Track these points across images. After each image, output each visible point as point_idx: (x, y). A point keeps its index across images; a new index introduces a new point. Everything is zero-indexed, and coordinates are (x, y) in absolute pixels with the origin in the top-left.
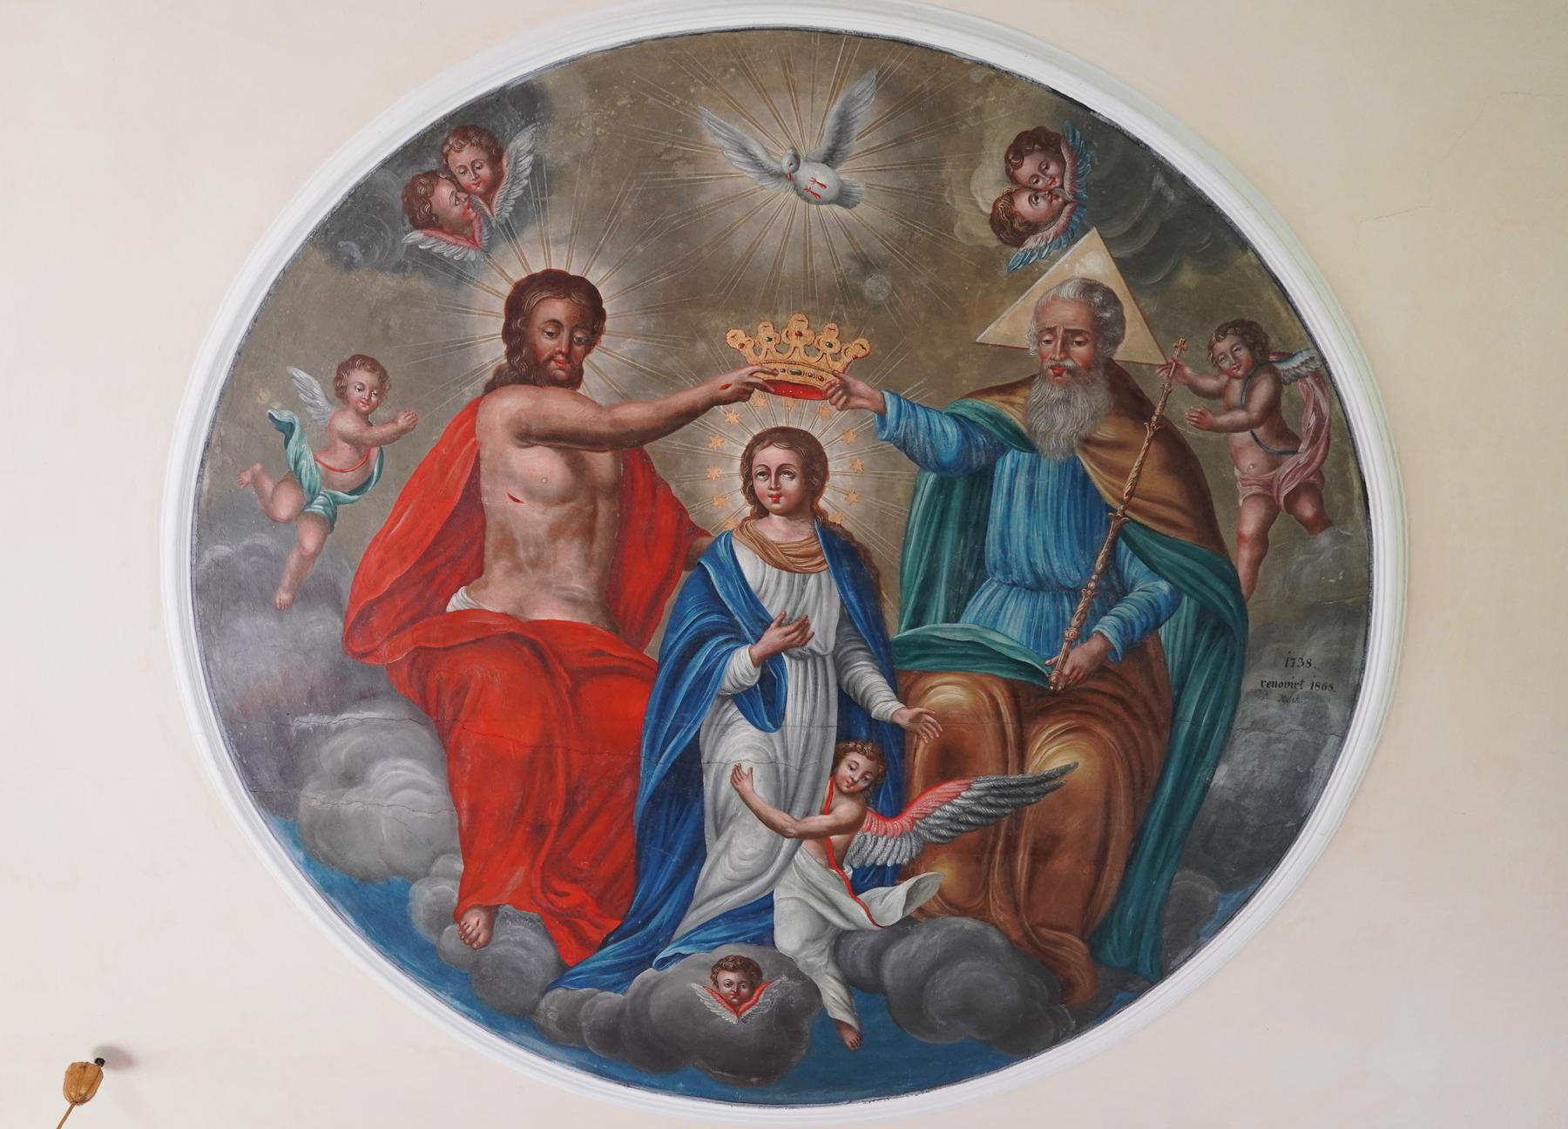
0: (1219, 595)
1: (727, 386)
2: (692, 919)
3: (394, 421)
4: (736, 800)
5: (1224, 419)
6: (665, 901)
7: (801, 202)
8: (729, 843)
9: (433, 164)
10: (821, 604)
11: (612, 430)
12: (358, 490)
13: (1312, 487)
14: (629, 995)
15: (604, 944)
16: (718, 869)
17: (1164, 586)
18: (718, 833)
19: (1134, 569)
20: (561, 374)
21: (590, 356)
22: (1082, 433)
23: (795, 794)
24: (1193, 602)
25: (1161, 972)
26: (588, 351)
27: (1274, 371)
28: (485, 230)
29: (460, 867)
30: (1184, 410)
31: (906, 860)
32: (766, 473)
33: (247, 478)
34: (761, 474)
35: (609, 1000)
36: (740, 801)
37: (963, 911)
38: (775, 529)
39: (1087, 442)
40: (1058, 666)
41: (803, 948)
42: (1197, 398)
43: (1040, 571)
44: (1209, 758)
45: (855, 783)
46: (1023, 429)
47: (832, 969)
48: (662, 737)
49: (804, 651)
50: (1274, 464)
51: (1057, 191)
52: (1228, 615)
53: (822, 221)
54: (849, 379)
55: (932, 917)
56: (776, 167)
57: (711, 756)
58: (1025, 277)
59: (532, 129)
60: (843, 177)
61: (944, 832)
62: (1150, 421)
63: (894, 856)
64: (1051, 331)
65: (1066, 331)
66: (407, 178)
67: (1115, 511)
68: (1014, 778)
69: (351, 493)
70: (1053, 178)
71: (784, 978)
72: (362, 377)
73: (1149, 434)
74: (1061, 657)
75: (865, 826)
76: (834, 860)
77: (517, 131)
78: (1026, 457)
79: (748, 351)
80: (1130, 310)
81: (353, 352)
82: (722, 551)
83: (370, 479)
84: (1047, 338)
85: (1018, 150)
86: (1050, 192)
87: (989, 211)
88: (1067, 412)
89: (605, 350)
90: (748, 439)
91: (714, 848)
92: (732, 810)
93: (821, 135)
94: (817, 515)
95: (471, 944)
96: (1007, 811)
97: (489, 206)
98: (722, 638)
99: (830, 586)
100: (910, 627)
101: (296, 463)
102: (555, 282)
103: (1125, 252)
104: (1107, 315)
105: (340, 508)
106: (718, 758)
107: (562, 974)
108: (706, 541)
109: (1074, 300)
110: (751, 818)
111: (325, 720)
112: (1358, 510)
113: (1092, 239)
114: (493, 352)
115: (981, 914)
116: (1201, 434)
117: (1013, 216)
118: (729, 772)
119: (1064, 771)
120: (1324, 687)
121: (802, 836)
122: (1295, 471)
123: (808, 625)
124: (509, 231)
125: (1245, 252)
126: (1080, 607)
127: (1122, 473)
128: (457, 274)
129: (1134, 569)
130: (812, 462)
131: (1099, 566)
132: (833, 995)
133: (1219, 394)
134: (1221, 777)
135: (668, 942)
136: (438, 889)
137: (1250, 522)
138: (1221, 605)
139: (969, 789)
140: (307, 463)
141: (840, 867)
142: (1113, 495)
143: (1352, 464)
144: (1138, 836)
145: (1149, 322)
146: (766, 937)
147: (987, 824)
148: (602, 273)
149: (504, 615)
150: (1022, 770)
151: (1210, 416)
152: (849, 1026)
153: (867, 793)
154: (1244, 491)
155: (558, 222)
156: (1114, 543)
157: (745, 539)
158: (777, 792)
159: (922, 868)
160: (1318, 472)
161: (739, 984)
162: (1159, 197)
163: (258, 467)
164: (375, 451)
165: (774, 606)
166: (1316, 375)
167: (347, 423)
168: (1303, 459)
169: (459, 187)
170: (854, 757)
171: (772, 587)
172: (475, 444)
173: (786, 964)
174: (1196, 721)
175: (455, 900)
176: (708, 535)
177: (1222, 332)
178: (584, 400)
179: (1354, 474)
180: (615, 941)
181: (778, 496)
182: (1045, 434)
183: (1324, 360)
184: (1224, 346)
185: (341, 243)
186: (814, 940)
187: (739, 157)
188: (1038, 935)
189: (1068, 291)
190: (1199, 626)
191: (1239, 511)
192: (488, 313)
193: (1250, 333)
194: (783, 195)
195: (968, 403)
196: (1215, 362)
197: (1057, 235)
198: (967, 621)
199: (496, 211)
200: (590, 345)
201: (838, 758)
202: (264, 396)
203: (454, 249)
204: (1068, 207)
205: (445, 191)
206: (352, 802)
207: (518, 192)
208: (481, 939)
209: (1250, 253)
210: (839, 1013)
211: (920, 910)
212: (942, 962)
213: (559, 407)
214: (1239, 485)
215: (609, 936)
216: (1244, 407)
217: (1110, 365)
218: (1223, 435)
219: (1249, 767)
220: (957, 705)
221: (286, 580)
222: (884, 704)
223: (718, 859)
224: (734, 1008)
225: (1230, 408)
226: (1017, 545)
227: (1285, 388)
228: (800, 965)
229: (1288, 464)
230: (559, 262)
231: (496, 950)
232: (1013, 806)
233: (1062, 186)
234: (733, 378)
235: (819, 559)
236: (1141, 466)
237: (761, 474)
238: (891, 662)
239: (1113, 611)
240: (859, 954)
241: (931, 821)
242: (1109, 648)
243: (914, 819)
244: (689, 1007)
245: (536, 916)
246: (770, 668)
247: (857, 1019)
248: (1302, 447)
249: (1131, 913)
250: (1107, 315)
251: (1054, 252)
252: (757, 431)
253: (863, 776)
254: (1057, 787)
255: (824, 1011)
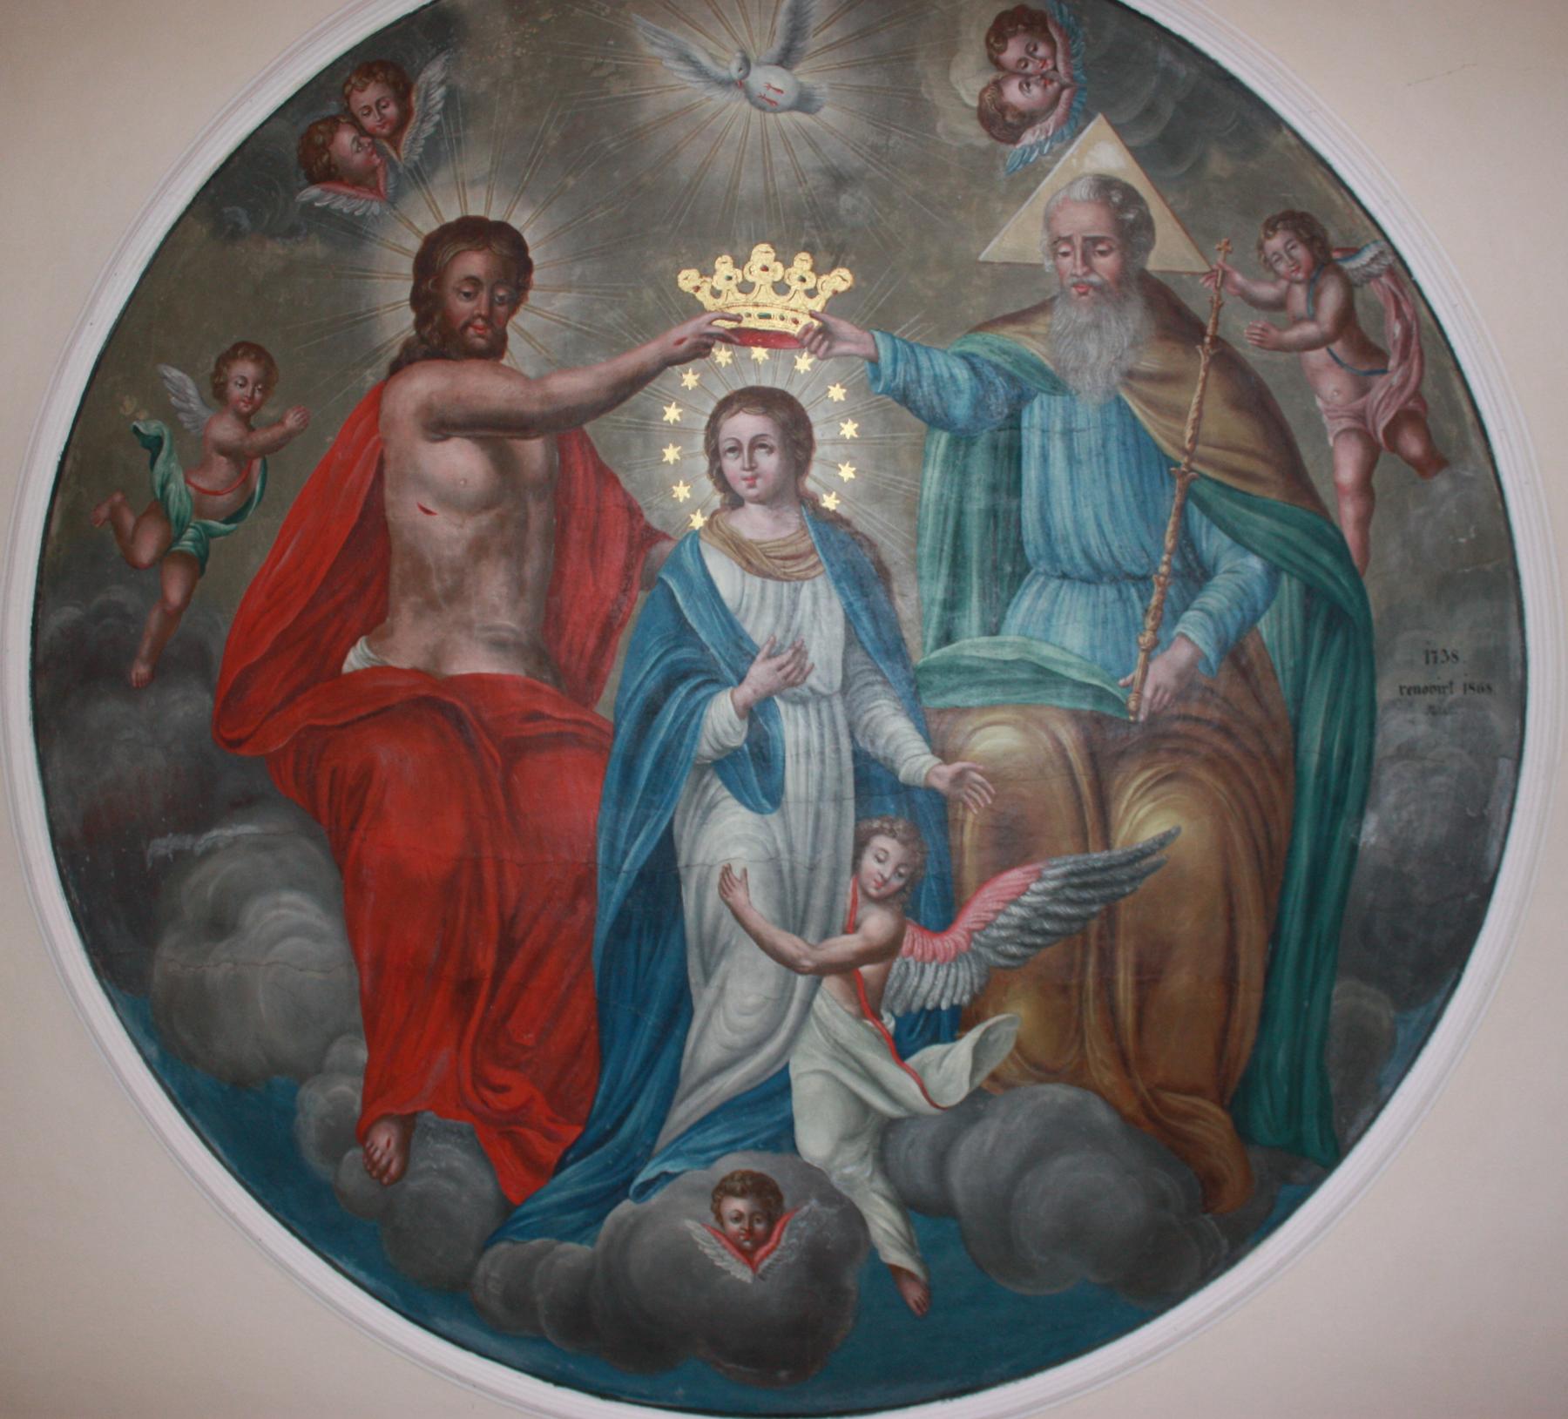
0: (1330, 574)
1: (680, 342)
2: (684, 1113)
3: (281, 422)
4: (728, 920)
5: (1293, 334)
6: (640, 1091)
7: (756, 113)
8: (722, 989)
9: (333, 108)
10: (819, 617)
11: (547, 409)
12: (235, 516)
13: (1411, 416)
14: (599, 1245)
15: (561, 1165)
16: (710, 1033)
17: (1255, 563)
18: (707, 975)
19: (1213, 542)
20: (480, 342)
21: (516, 318)
22: (1124, 365)
23: (805, 911)
24: (1295, 584)
25: (1335, 1152)
26: (513, 311)
27: (1339, 271)
28: (391, 179)
29: (362, 1055)
30: (1242, 329)
31: (966, 998)
32: (736, 449)
33: (104, 512)
34: (732, 450)
35: (575, 1252)
36: (733, 922)
37: (1048, 1074)
38: (754, 523)
39: (1130, 375)
40: (1136, 686)
41: (836, 1151)
42: (1255, 311)
43: (1096, 557)
44: (1351, 804)
45: (885, 882)
46: (1050, 366)
47: (879, 1184)
48: (624, 831)
49: (803, 691)
50: (1363, 390)
51: (1051, 75)
52: (1340, 595)
53: (783, 134)
54: (832, 320)
55: (1009, 1086)
56: (724, 74)
57: (690, 858)
58: (1033, 172)
59: (443, 58)
60: (802, 79)
61: (1013, 949)
62: (1202, 343)
63: (949, 993)
64: (1068, 240)
65: (1085, 239)
66: (303, 126)
67: (1178, 465)
68: (1098, 857)
69: (227, 522)
70: (1044, 60)
71: (814, 1203)
72: (246, 369)
73: (1204, 360)
74: (1137, 673)
75: (905, 948)
76: (868, 1004)
77: (427, 62)
78: (1058, 403)
79: (704, 297)
80: (1157, 209)
81: (236, 338)
82: (688, 559)
83: (250, 500)
84: (1064, 249)
85: (999, 32)
86: (1043, 76)
87: (975, 104)
88: (1101, 340)
89: (533, 310)
90: (711, 407)
91: (703, 999)
92: (723, 937)
93: (773, 33)
94: (809, 503)
95: (380, 1177)
96: (1095, 908)
97: (396, 149)
98: (700, 679)
99: (830, 598)
100: (938, 645)
101: (163, 487)
102: (472, 231)
103: (1138, 140)
104: (1131, 216)
105: (213, 543)
106: (699, 857)
107: (506, 1219)
108: (666, 547)
109: (1089, 201)
110: (749, 949)
111: (187, 842)
112: (1475, 441)
113: (1098, 127)
114: (398, 322)
115: (1077, 1077)
116: (1266, 355)
117: (1003, 108)
118: (715, 878)
119: (1164, 841)
120: (1481, 689)
121: (821, 971)
122: (1390, 394)
123: (805, 654)
124: (418, 176)
125: (1280, 130)
126: (1154, 601)
127: (1179, 414)
128: (353, 232)
129: (1213, 542)
130: (794, 429)
131: (1169, 543)
132: (884, 1223)
133: (1280, 304)
134: (1370, 832)
135: (648, 1155)
136: (336, 1092)
137: (1347, 465)
138: (1329, 583)
139: (1040, 879)
140: (176, 487)
141: (877, 1017)
142: (1174, 445)
143: (1457, 384)
144: (1275, 936)
145: (1178, 218)
146: (783, 1138)
147: (1071, 934)
148: (527, 215)
149: (414, 672)
150: (1107, 844)
151: (1274, 332)
152: (911, 1275)
153: (904, 896)
154: (1333, 427)
155: (477, 161)
156: (1182, 511)
157: (715, 541)
158: (781, 904)
159: (990, 1012)
160: (1417, 395)
161: (752, 1215)
162: (1168, 76)
163: (118, 497)
164: (257, 463)
165: (760, 628)
166: (1391, 272)
167: (225, 430)
168: (1396, 380)
169: (362, 131)
170: (882, 843)
171: (755, 604)
172: (380, 441)
173: (815, 1179)
174: (1325, 754)
175: (357, 1108)
176: (666, 537)
177: (1271, 227)
178: (512, 373)
179: (1460, 393)
180: (577, 1159)
181: (754, 478)
182: (1076, 370)
183: (1396, 253)
184: (1276, 243)
185: (226, 210)
186: (849, 1137)
187: (681, 66)
188: (1157, 1101)
189: (1082, 191)
190: (1308, 617)
191: (1330, 453)
192: (397, 276)
193: (1304, 226)
194: (734, 105)
195: (978, 337)
196: (1269, 265)
197: (1057, 126)
198: (1010, 634)
199: (403, 154)
200: (515, 303)
201: (861, 844)
202: (129, 405)
203: (356, 203)
204: (1065, 94)
205: (346, 138)
206: (219, 964)
207: (429, 129)
208: (394, 1168)
209: (1285, 131)
210: (895, 1256)
211: (994, 1077)
212: (1035, 1157)
213: (483, 387)
214: (1325, 418)
215: (566, 1153)
216: (1312, 318)
217: (1145, 278)
218: (1295, 354)
219: (1405, 815)
220: (1008, 754)
221: (145, 648)
222: (914, 759)
223: (709, 1015)
224: (748, 1256)
225: (1297, 321)
226: (1061, 516)
227: (1358, 293)
228: (834, 1179)
229: (1379, 388)
230: (478, 207)
231: (414, 1185)
232: (1103, 900)
233: (1055, 68)
234: (687, 330)
235: (812, 560)
236: (1200, 403)
237: (732, 450)
238: (915, 691)
239: (1196, 604)
240: (914, 1154)
241: (995, 933)
242: (1199, 654)
243: (970, 931)
244: (686, 1261)
245: (465, 1125)
246: (757, 713)
247: (923, 1262)
248: (1392, 363)
249: (1281, 1059)
250: (1131, 216)
251: (1057, 146)
252: (722, 394)
253: (896, 870)
254: (1155, 867)
255: (873, 1252)
